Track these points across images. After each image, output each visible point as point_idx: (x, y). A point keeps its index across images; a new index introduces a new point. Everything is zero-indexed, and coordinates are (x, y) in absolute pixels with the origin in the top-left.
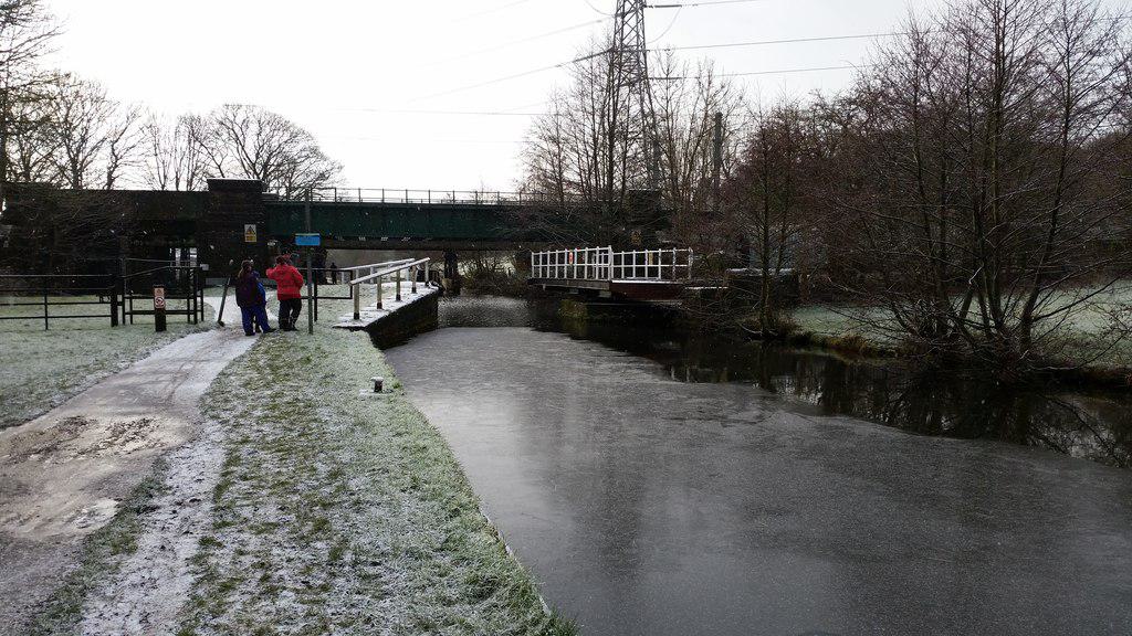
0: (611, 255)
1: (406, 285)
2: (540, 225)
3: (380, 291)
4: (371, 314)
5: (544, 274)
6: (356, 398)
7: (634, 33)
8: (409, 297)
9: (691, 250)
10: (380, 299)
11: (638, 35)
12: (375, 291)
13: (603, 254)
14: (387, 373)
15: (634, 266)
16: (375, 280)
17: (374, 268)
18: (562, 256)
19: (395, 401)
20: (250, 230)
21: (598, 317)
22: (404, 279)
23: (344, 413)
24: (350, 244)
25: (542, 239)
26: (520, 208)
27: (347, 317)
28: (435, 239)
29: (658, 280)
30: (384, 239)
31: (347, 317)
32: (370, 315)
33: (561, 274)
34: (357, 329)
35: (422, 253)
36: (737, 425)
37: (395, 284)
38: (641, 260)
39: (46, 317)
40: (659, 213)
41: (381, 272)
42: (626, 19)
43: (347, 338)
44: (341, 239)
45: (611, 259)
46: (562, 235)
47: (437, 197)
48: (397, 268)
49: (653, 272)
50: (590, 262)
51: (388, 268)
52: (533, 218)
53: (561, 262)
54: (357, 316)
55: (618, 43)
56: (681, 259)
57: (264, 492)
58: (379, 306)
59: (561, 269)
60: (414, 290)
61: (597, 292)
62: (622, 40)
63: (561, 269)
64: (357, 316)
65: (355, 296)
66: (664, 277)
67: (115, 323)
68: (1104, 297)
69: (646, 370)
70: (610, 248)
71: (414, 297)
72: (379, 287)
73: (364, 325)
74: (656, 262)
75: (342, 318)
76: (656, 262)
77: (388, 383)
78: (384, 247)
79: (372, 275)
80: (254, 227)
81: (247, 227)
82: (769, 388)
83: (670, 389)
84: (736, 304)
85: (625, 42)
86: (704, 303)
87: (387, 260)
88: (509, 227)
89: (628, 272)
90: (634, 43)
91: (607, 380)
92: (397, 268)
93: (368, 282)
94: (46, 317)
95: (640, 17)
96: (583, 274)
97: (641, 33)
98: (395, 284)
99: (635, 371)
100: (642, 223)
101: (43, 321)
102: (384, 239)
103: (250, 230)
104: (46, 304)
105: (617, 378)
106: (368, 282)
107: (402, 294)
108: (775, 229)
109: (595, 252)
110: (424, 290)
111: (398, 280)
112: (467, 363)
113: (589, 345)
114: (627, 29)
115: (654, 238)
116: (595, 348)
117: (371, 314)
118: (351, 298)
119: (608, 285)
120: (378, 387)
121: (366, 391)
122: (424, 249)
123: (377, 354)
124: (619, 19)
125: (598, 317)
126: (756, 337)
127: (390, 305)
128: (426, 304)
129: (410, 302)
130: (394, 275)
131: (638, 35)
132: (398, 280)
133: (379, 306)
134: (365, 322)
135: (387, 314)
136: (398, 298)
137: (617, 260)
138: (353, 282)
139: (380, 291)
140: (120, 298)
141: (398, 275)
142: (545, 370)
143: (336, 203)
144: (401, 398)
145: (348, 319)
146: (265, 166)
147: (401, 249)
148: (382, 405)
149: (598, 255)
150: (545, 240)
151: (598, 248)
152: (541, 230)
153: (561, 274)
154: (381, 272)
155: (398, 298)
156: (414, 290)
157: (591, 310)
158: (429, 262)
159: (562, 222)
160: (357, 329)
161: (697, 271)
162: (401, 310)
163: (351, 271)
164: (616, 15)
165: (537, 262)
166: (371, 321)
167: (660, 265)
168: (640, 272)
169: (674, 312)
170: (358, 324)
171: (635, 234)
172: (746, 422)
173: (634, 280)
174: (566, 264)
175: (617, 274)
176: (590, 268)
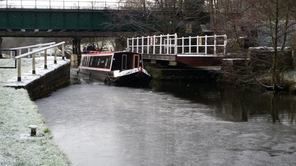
0: (176, 39)
1: (50, 59)
2: (132, 22)
3: (34, 62)
4: (28, 77)
5: (135, 50)
6: (17, 141)
8: (52, 67)
9: (225, 36)
10: (34, 68)
12: (31, 63)
13: (171, 39)
14: (40, 120)
16: (31, 56)
17: (31, 48)
18: (146, 40)
19: (45, 143)
21: (169, 77)
22: (49, 55)
23: (9, 155)
24: (16, 33)
25: (133, 30)
26: (118, 11)
27: (13, 80)
28: (67, 31)
29: (206, 55)
30: (37, 30)
31: (13, 80)
32: (28, 78)
33: (145, 51)
34: (20, 87)
35: (59, 39)
36: (281, 154)
37: (43, 58)
38: (194, 42)
40: (203, 14)
41: (35, 51)
43: (13, 94)
44: (10, 30)
45: (176, 42)
46: (144, 27)
47: (57, 8)
48: (45, 48)
49: (202, 50)
50: (163, 44)
51: (39, 48)
52: (127, 18)
53: (145, 43)
54: (19, 79)
56: (220, 41)
58: (34, 72)
59: (145, 48)
60: (55, 62)
61: (168, 62)
63: (145, 48)
64: (19, 79)
65: (18, 66)
66: (208, 53)
69: (207, 113)
70: (176, 35)
71: (56, 67)
72: (34, 60)
73: (24, 85)
74: (203, 43)
75: (9, 80)
76: (203, 43)
77: (40, 129)
78: (37, 36)
79: (29, 53)
82: (275, 118)
83: (226, 127)
84: (256, 69)
86: (236, 69)
87: (38, 43)
88: (113, 23)
89: (187, 50)
91: (181, 121)
92: (45, 48)
93: (27, 57)
96: (152, 50)
99: (199, 114)
100: (193, 20)
102: (37, 30)
105: (188, 119)
106: (27, 57)
107: (48, 64)
108: (282, 22)
109: (166, 37)
110: (61, 62)
111: (45, 55)
112: (90, 109)
113: (166, 96)
115: (200, 29)
116: (170, 98)
117: (28, 77)
118: (16, 68)
119: (174, 57)
120: (33, 133)
121: (25, 135)
122: (62, 37)
123: (32, 106)
125: (169, 77)
126: (270, 89)
127: (41, 72)
128: (63, 71)
129: (53, 69)
130: (43, 52)
132: (45, 55)
133: (34, 72)
134: (25, 83)
135: (39, 77)
136: (46, 67)
137: (180, 43)
138: (17, 57)
139: (34, 62)
141: (46, 52)
142: (141, 113)
143: (7, 9)
144: (50, 141)
145: (14, 81)
147: (48, 37)
148: (36, 147)
149: (168, 39)
150: (134, 31)
151: (168, 35)
152: (132, 25)
153: (145, 51)
154: (35, 51)
155: (46, 67)
156: (55, 62)
157: (164, 73)
158: (64, 44)
159: (145, 20)
160: (20, 87)
161: (229, 48)
162: (48, 75)
163: (16, 50)
165: (130, 44)
166: (29, 82)
167: (206, 45)
168: (194, 50)
169: (217, 74)
170: (20, 84)
171: (189, 27)
173: (198, 55)
174: (148, 45)
175: (180, 50)
176: (163, 47)
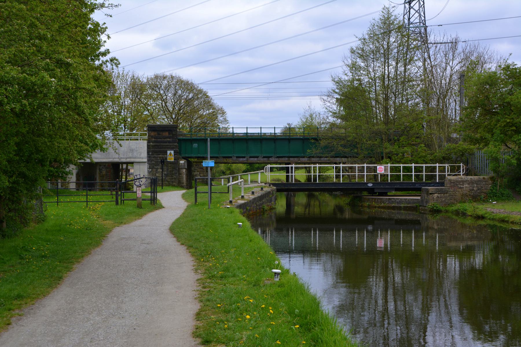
7: (417, 15)
11: (420, 15)
15: (402, 173)
20: (170, 154)
39: (87, 202)
42: (412, 5)
55: (406, 21)
57: (190, 123)
62: (409, 19)
67: (117, 203)
68: (507, 190)
80: (172, 152)
81: (169, 152)
85: (411, 20)
90: (417, 21)
94: (87, 202)
95: (422, 3)
97: (422, 14)
98: (56, 190)
101: (85, 204)
103: (170, 154)
104: (87, 195)
114: (412, 12)
124: (407, 6)
129: (260, 195)
131: (420, 15)
140: (120, 193)
146: (178, 114)
164: (405, 3)
172: (455, 267)
